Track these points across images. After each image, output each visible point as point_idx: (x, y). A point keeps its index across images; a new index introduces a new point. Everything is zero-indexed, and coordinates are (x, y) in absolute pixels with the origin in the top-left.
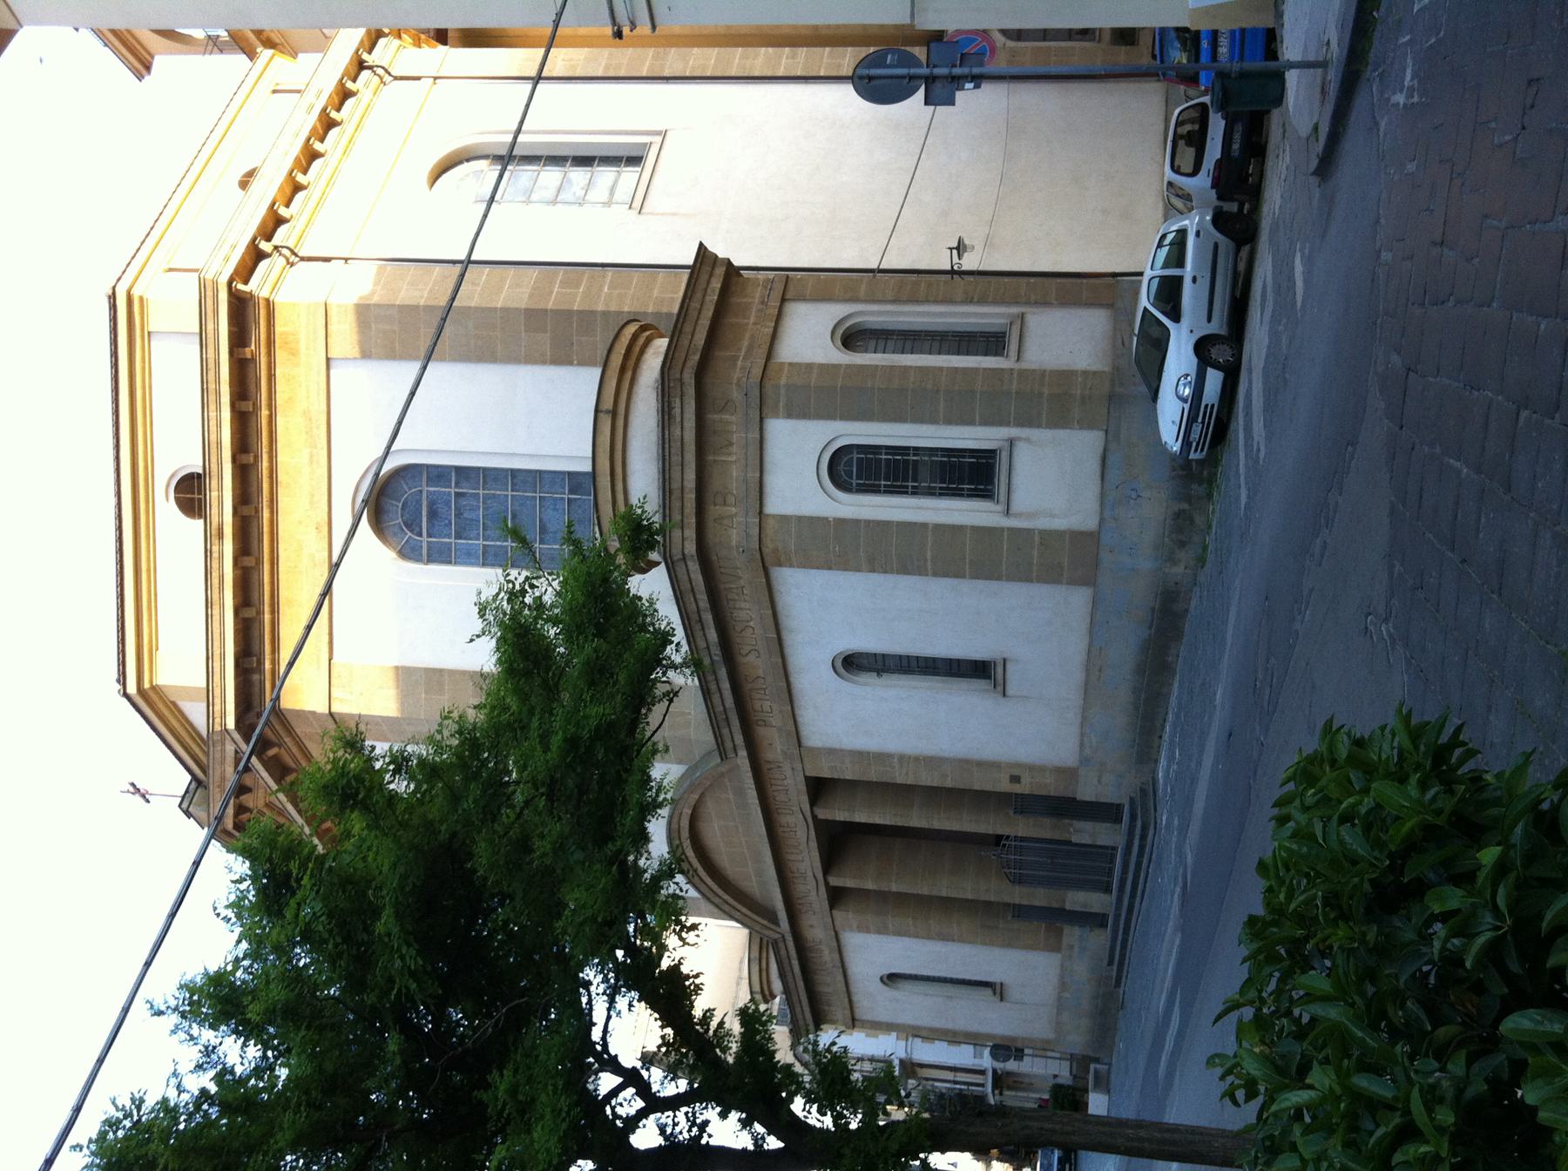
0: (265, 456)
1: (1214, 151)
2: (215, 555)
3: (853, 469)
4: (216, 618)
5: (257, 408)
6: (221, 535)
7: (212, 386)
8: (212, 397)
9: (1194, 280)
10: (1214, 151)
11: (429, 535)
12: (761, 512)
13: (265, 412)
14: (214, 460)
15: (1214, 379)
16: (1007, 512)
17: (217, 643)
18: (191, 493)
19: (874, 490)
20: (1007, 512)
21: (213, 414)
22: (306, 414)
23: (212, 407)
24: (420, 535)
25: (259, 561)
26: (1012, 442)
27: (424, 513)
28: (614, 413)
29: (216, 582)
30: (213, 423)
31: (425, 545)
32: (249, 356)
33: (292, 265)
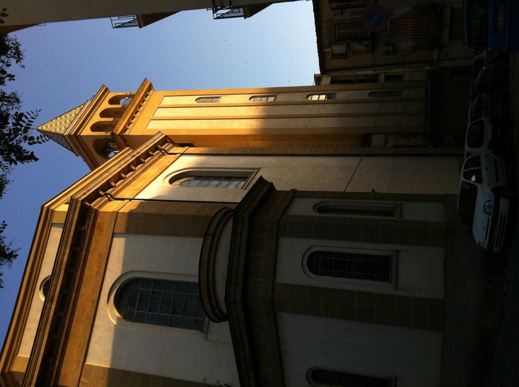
0: (79, 271)
1: (488, 136)
2: (48, 309)
3: (317, 263)
4: (40, 337)
5: (81, 250)
6: (52, 301)
7: (65, 239)
8: (64, 243)
9: (487, 169)
10: (488, 136)
11: (138, 310)
12: (274, 281)
13: (84, 253)
14: (58, 268)
15: (504, 204)
16: (396, 287)
17: (37, 349)
18: (47, 286)
19: (329, 274)
20: (396, 287)
21: (62, 250)
22: (100, 254)
23: (63, 247)
24: (134, 309)
25: (66, 315)
26: (397, 252)
27: (138, 299)
28: (213, 236)
29: (45, 320)
30: (62, 253)
31: (135, 313)
32: (83, 229)
33: (110, 201)
